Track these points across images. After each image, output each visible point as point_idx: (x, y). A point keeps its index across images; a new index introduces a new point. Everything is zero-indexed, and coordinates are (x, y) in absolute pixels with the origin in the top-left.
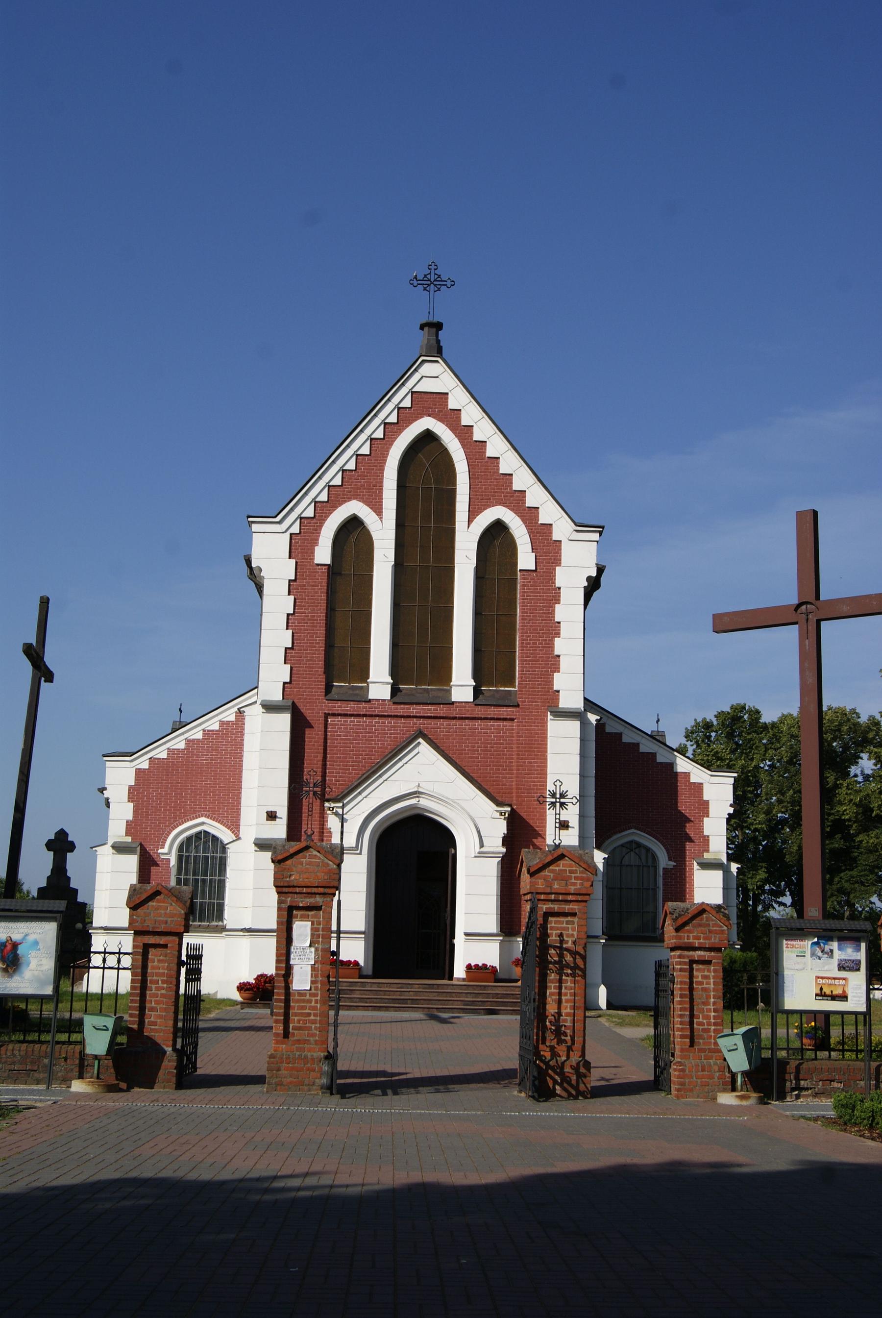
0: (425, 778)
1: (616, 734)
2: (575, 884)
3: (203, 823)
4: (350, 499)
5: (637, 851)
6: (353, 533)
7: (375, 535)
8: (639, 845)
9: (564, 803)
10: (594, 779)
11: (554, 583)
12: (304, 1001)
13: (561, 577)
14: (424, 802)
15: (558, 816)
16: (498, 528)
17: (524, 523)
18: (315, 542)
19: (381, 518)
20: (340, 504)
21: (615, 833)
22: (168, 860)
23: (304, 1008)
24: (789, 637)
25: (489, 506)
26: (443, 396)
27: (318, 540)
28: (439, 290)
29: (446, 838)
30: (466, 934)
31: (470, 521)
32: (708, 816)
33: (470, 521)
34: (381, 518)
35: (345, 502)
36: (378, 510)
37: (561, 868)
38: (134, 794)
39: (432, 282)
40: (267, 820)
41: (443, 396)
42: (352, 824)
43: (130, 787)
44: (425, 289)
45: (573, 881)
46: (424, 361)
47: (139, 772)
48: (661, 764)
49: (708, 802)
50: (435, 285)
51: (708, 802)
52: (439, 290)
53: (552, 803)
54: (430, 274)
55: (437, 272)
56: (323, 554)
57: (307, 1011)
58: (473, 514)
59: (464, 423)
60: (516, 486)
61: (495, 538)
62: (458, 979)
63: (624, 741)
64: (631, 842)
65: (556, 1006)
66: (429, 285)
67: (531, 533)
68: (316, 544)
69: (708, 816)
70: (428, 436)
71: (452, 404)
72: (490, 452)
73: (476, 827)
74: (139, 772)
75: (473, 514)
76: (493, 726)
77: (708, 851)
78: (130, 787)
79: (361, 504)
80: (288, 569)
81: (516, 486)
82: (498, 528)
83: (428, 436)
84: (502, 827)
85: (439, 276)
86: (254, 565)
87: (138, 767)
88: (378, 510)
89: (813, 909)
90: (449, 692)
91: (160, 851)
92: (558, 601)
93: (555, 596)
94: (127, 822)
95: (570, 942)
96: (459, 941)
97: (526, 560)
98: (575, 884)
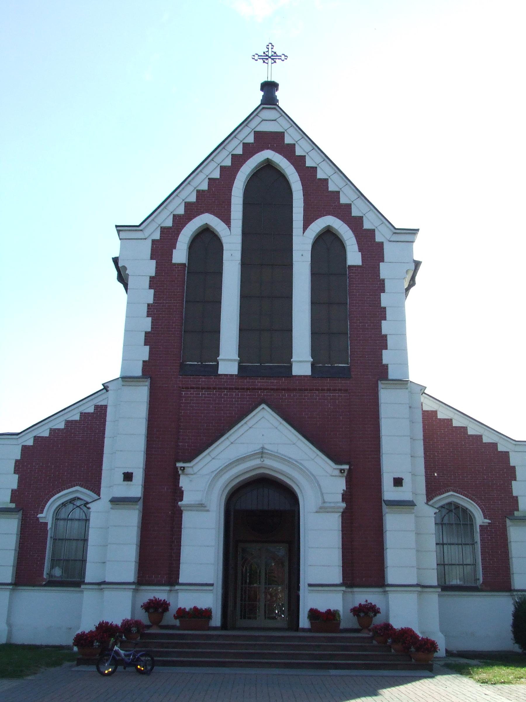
1: (432, 411)
3: (77, 491)
4: (202, 213)
6: (207, 244)
7: (224, 240)
8: (457, 507)
10: (422, 443)
11: (379, 276)
14: (268, 462)
19: (229, 227)
20: (195, 217)
22: (46, 524)
25: (321, 216)
27: (176, 245)
28: (275, 62)
29: (289, 495)
30: (310, 585)
32: (515, 480)
34: (229, 227)
35: (199, 215)
36: (227, 221)
39: (269, 57)
40: (124, 480)
42: (206, 483)
43: (17, 461)
44: (264, 62)
46: (263, 108)
48: (472, 436)
50: (273, 59)
54: (268, 51)
55: (273, 50)
56: (180, 255)
58: (306, 226)
61: (327, 241)
62: (304, 630)
64: (450, 504)
65: (109, 594)
69: (515, 480)
70: (268, 165)
73: (319, 485)
75: (306, 226)
76: (330, 396)
77: (517, 510)
78: (17, 461)
80: (150, 268)
83: (268, 165)
84: (341, 485)
85: (275, 53)
86: (120, 265)
87: (25, 444)
88: (227, 221)
90: (290, 368)
91: (39, 516)
94: (12, 490)
97: (354, 257)
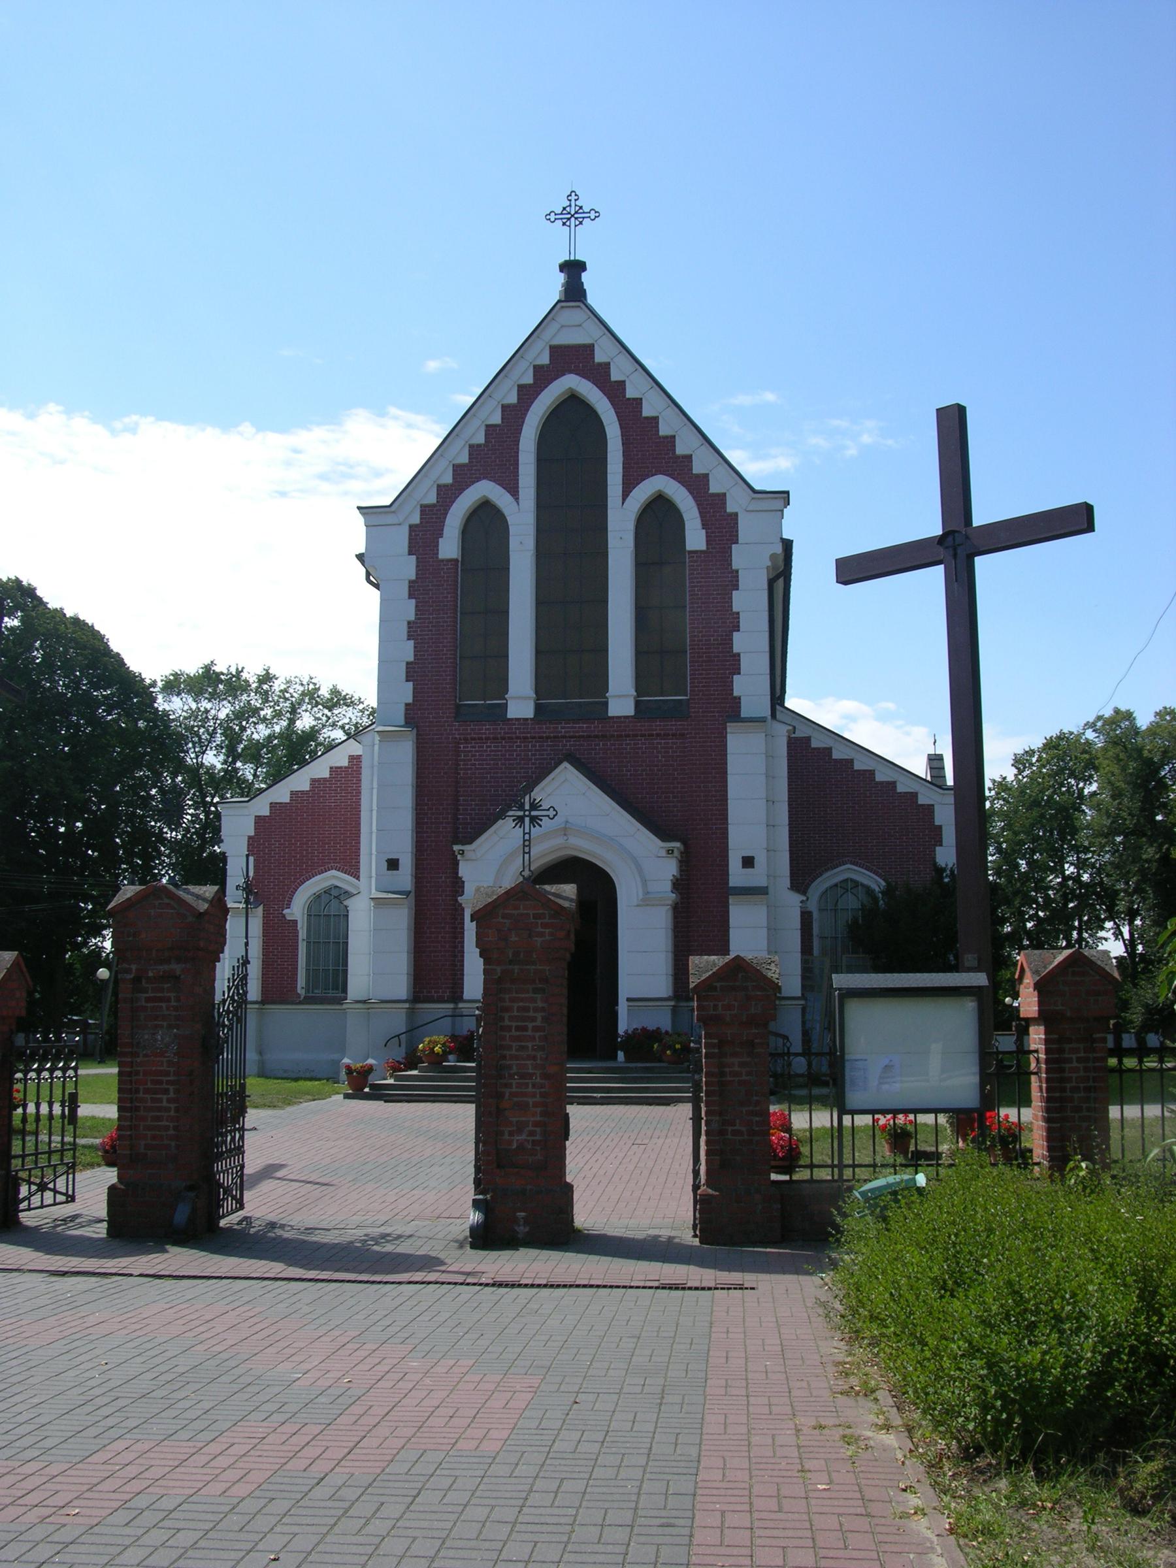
0: (577, 812)
2: (542, 935)
4: (478, 479)
5: (854, 891)
6: (487, 524)
8: (856, 884)
9: (537, 817)
12: (159, 1109)
13: (740, 557)
15: (527, 837)
16: (659, 506)
17: (691, 493)
18: (439, 533)
19: (517, 499)
21: (826, 870)
23: (158, 1119)
24: (931, 582)
25: (647, 476)
26: (589, 349)
31: (625, 495)
33: (625, 495)
34: (517, 499)
37: (521, 911)
38: (254, 845)
41: (589, 349)
43: (250, 838)
45: (540, 929)
47: (259, 820)
48: (882, 783)
49: (940, 827)
51: (940, 827)
52: (581, 223)
53: (519, 817)
56: (449, 547)
57: (164, 1123)
59: (613, 378)
60: (680, 450)
61: (658, 519)
63: (834, 757)
64: (846, 880)
66: (569, 219)
67: (700, 505)
68: (441, 535)
69: (941, 845)
70: (573, 400)
71: (599, 358)
72: (647, 412)
74: (259, 820)
78: (250, 838)
79: (492, 484)
81: (680, 450)
82: (659, 506)
84: (669, 869)
88: (513, 490)
89: (970, 956)
90: (606, 704)
92: (736, 587)
93: (732, 581)
95: (539, 1019)
96: (623, 1008)
97: (695, 538)
98: (542, 935)
